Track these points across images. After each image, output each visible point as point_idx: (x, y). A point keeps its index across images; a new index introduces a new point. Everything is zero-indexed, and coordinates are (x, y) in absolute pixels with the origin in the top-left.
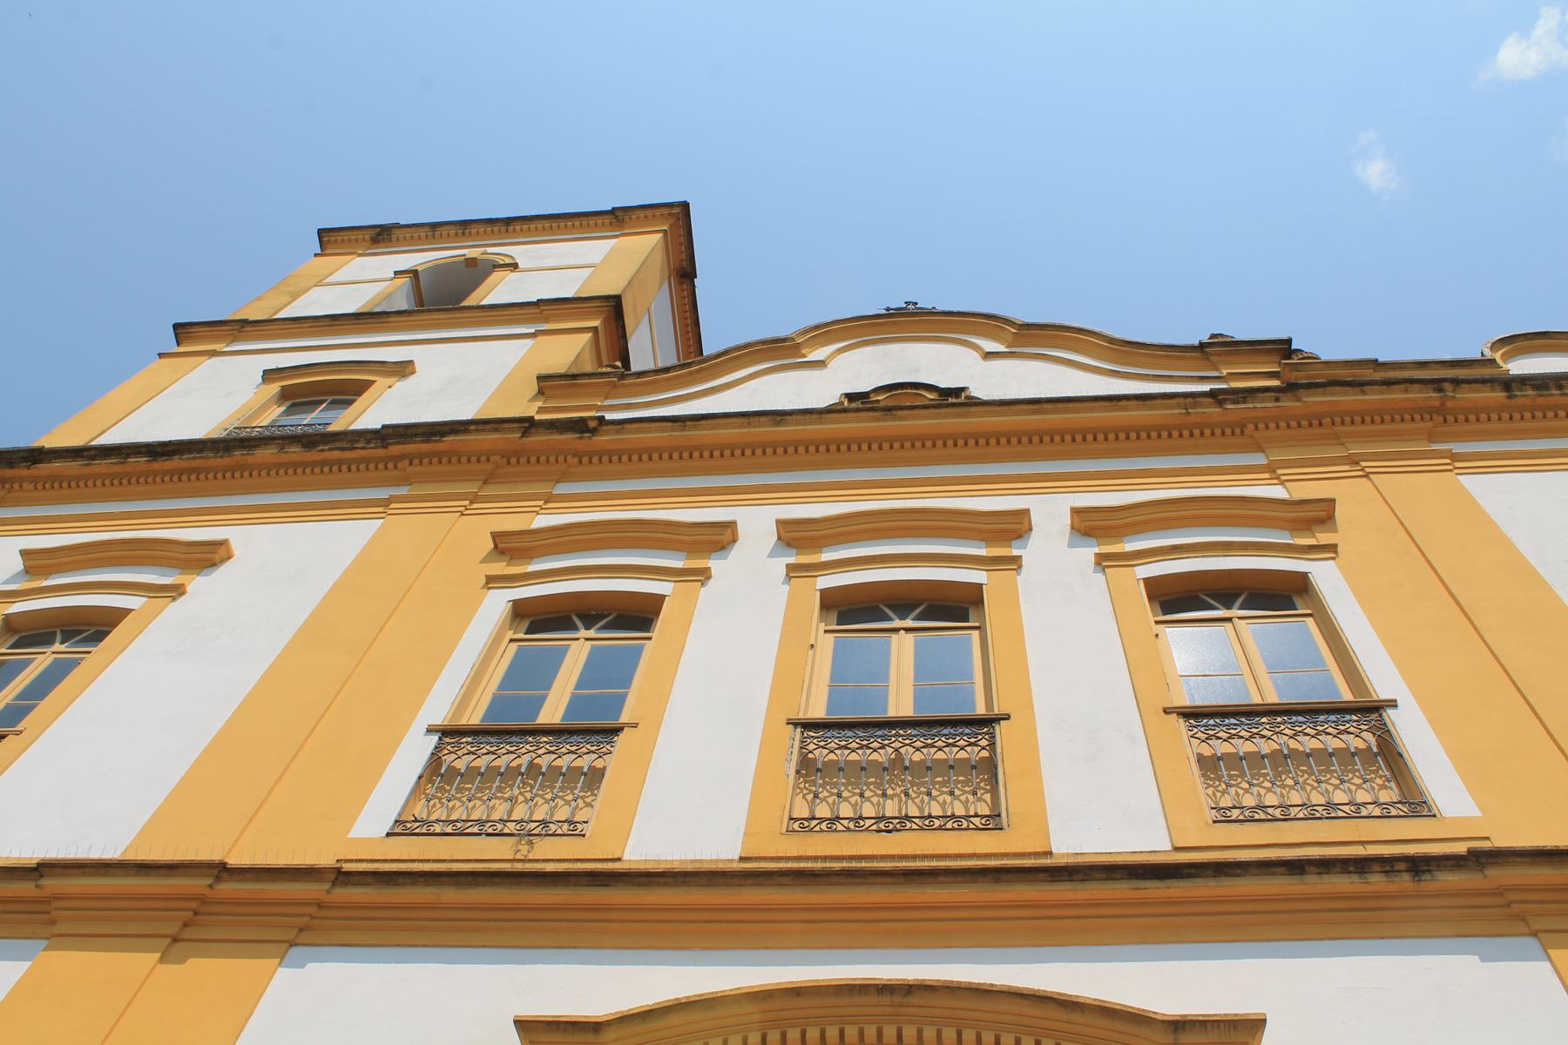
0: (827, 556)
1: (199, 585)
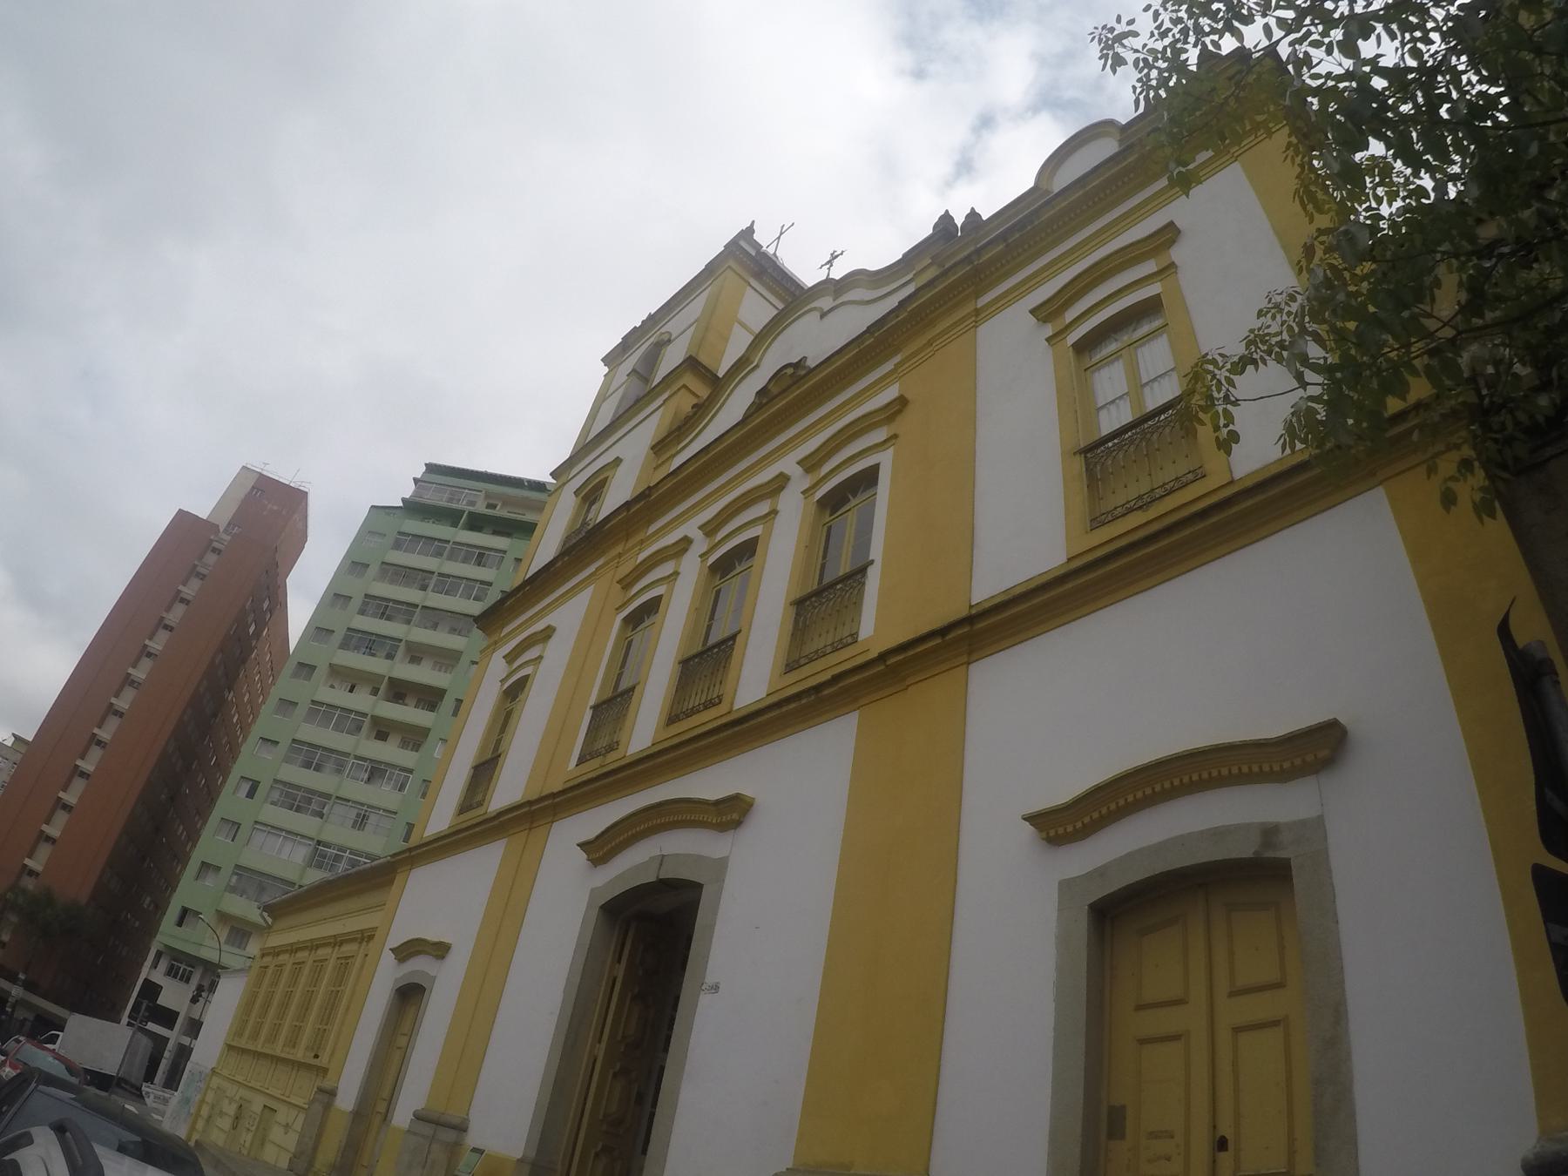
0: (1071, 315)
1: (1177, 254)
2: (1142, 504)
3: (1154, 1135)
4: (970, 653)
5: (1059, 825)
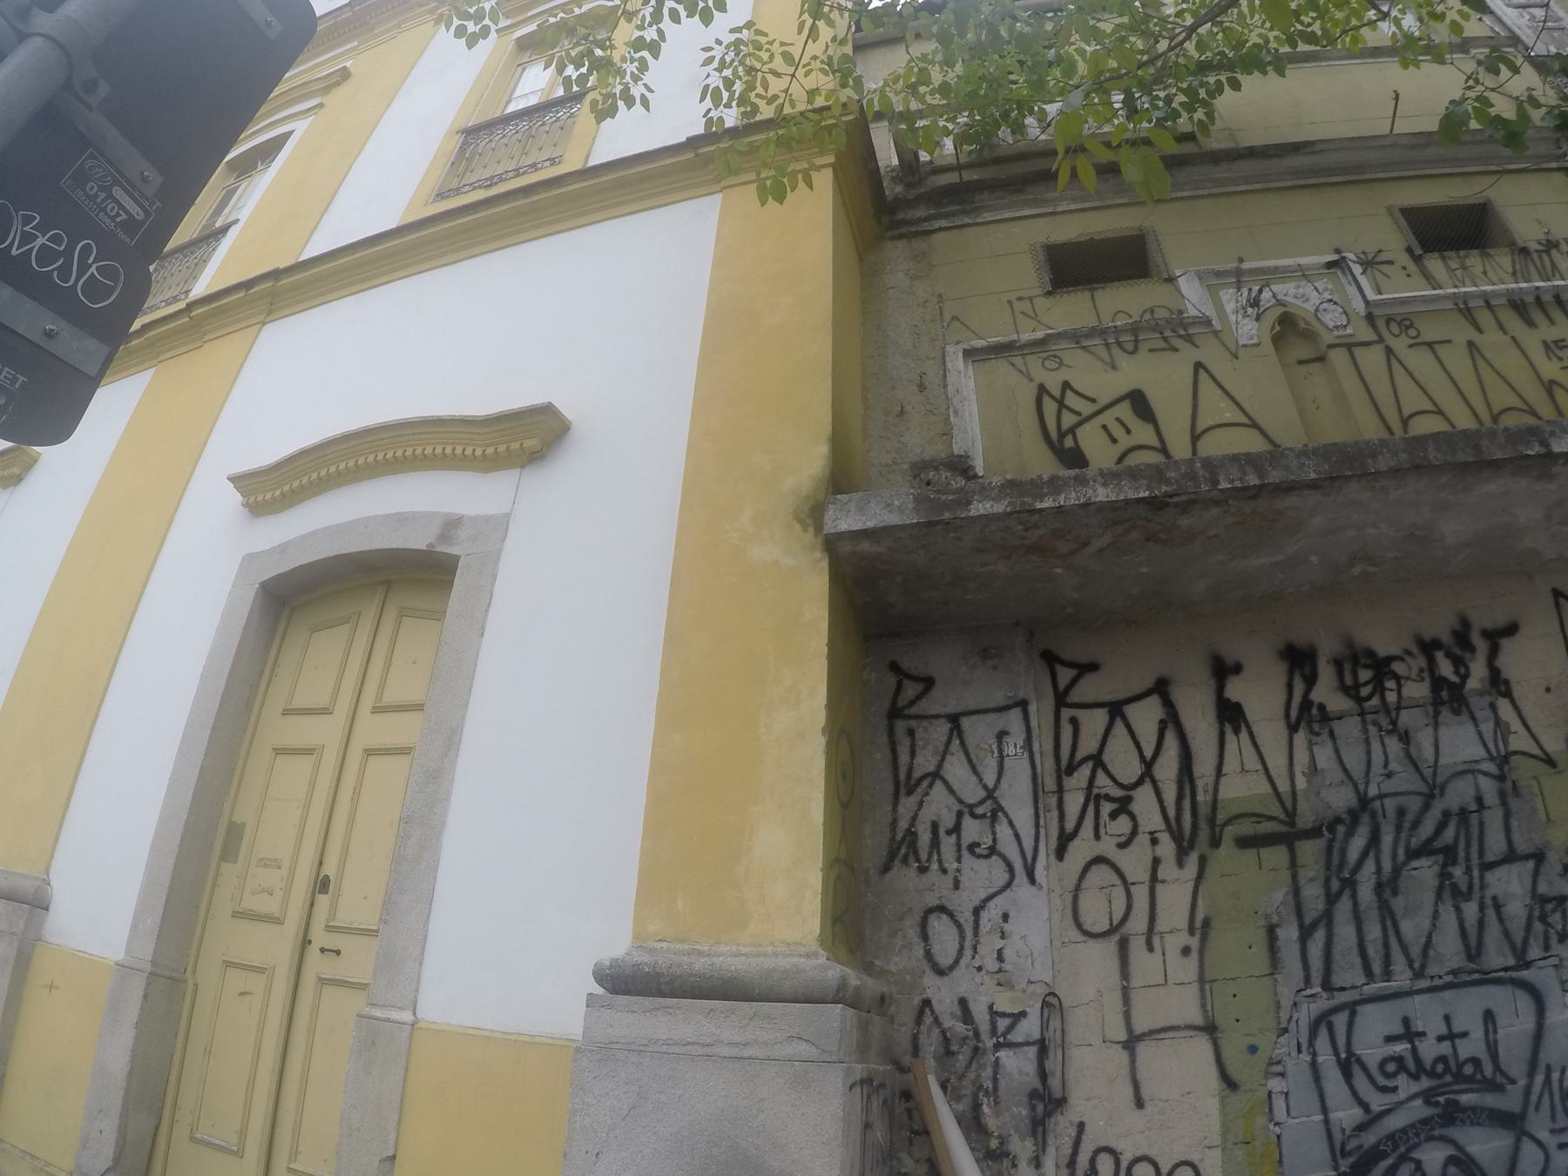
2: (490, 182)
3: (265, 863)
4: (269, 313)
5: (269, 489)
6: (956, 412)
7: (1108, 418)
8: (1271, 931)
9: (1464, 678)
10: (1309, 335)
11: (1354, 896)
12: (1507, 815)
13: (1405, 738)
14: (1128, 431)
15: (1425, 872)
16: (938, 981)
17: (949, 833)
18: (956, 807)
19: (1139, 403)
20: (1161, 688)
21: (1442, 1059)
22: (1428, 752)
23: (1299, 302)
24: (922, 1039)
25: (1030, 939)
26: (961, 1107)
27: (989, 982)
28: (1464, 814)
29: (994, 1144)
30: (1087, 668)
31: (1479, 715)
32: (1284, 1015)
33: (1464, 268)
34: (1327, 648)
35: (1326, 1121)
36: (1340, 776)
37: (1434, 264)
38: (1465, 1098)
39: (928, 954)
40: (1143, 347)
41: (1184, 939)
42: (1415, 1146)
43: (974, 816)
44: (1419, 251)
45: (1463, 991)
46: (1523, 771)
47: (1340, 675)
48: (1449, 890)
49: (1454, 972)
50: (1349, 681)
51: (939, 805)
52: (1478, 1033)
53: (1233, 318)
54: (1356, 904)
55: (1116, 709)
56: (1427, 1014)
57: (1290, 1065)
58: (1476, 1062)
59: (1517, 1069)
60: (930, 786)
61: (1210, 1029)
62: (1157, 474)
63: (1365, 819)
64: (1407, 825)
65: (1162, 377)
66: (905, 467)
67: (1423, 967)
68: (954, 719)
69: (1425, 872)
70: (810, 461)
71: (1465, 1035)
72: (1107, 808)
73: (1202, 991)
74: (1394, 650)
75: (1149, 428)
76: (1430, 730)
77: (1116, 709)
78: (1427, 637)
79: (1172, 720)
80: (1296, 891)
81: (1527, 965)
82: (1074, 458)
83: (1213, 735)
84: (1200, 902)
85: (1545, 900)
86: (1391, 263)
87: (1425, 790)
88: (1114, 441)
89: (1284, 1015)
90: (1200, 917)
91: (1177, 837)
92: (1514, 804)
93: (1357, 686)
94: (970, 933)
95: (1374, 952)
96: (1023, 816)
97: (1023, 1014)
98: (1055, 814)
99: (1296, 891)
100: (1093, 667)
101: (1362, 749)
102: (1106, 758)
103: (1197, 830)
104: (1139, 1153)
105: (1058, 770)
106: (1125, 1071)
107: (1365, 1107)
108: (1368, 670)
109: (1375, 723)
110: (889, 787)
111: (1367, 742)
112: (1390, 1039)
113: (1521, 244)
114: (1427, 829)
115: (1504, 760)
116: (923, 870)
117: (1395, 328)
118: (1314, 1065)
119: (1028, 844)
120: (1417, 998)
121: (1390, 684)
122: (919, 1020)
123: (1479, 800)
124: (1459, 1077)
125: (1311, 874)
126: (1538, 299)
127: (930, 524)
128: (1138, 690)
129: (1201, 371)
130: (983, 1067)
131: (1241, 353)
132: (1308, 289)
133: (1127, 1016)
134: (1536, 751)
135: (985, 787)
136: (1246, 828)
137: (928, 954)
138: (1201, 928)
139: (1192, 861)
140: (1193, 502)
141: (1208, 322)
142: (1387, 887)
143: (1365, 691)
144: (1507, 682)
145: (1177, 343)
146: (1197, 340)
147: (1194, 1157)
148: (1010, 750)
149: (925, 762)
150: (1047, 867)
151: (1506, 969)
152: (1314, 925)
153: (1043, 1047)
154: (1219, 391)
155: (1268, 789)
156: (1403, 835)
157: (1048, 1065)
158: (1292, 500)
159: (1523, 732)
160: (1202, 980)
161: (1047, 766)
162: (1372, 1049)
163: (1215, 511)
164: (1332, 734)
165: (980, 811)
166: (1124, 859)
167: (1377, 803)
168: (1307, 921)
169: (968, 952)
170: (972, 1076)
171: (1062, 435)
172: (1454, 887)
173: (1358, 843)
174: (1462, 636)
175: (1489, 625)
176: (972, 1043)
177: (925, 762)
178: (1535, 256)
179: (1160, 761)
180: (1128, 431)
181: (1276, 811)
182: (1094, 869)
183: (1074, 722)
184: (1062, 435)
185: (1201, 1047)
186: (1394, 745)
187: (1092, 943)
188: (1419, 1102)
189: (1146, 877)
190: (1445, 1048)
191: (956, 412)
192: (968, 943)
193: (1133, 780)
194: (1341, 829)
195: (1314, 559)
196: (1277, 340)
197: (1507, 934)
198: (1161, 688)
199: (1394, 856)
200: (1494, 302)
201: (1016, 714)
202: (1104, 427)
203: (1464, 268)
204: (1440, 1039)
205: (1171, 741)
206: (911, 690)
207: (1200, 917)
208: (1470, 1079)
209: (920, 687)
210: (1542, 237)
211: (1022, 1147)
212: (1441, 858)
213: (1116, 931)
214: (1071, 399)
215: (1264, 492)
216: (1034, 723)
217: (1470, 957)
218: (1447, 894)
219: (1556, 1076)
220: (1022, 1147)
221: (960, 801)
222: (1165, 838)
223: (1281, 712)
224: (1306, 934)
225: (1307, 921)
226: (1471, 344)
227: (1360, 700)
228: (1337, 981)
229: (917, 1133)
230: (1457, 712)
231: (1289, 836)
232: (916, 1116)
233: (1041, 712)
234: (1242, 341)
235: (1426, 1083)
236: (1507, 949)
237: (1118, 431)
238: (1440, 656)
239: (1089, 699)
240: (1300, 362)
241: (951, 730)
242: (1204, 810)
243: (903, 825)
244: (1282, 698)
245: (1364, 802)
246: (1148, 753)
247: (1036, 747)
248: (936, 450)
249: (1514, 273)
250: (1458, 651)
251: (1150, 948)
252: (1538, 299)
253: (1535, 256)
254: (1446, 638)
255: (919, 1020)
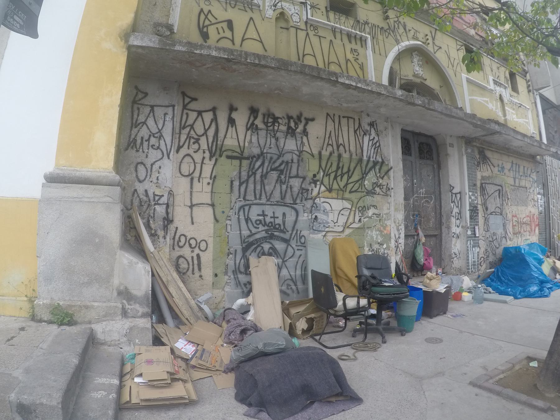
6: (173, 9)
7: (219, 26)
8: (232, 182)
9: (297, 128)
10: (287, 21)
11: (255, 177)
12: (298, 166)
13: (277, 139)
14: (224, 32)
15: (274, 175)
16: (139, 184)
17: (146, 141)
18: (149, 133)
19: (230, 24)
20: (214, 110)
21: (271, 222)
22: (282, 145)
23: (288, 10)
24: (134, 200)
25: (167, 175)
26: (144, 221)
27: (154, 186)
28: (287, 163)
29: (153, 232)
30: (194, 99)
31: (298, 139)
32: (232, 205)
33: (339, 19)
34: (262, 110)
35: (240, 233)
36: (258, 145)
37: (331, 15)
38: (275, 233)
39: (137, 176)
40: (237, 7)
41: (208, 180)
42: (262, 243)
43: (154, 137)
44: (329, 9)
45: (279, 207)
46: (305, 156)
47: (264, 118)
48: (279, 181)
49: (277, 202)
50: (266, 121)
51: (144, 132)
52: (281, 218)
53: (267, 8)
54: (255, 179)
55: (200, 113)
56: (269, 211)
57: (232, 217)
58: (279, 225)
59: (289, 229)
60: (142, 126)
61: (213, 205)
62: (231, 52)
63: (262, 158)
64: (272, 162)
65: (240, 18)
66: (152, 23)
67: (269, 199)
68: (152, 107)
69: (274, 175)
70: (128, 19)
71: (278, 218)
72: (192, 141)
73: (212, 195)
74: (280, 116)
75: (231, 33)
76: (284, 139)
77: (200, 113)
78: (290, 115)
79: (215, 119)
80: (240, 173)
81: (296, 204)
82: (205, 36)
83: (226, 126)
84: (214, 171)
85: (303, 189)
86: (319, 9)
87: (278, 153)
88: (219, 33)
89: (232, 205)
90: (213, 175)
91: (210, 152)
92: (301, 164)
93: (268, 122)
94: (149, 171)
95: (258, 192)
96: (168, 139)
97: (163, 196)
98: (178, 140)
99: (240, 173)
100: (196, 99)
101: (265, 139)
102: (194, 126)
103: (216, 151)
104: (192, 237)
105: (180, 128)
106: (189, 214)
107: (251, 231)
108: (272, 119)
109: (270, 133)
110: (130, 124)
111: (267, 138)
112: (258, 215)
113: (358, 19)
114: (277, 164)
115: (301, 152)
116: (137, 151)
117: (312, 28)
118: (239, 218)
119: (169, 147)
120: (267, 206)
121: (277, 124)
122: (133, 195)
123: (292, 160)
124: (275, 228)
125: (245, 169)
126: (355, 36)
127: (162, 49)
128: (207, 109)
129: (252, 22)
130: (151, 210)
131: (265, 19)
132: (292, 7)
133: (191, 199)
134: (310, 152)
135: (158, 129)
136: (230, 153)
137: (137, 176)
138: (214, 178)
139: (214, 160)
140: (238, 62)
141: (259, 7)
142: (264, 176)
143: (269, 125)
144: (307, 133)
145: (247, 9)
146: (254, 10)
147: (206, 239)
148: (167, 119)
149: (142, 119)
150: (173, 155)
151: (290, 204)
152: (243, 182)
153: (168, 205)
154: (254, 28)
155: (238, 144)
156: (271, 164)
157: (169, 211)
158: (266, 70)
159: (308, 146)
160: (212, 192)
161: (177, 125)
162: (254, 218)
163: (244, 66)
164: (258, 134)
165: (156, 135)
166: (195, 156)
167: (266, 155)
168: (242, 181)
169: (148, 177)
170: (147, 212)
171: (204, 27)
172: (281, 180)
173: (258, 164)
174: (299, 118)
175: (307, 117)
176: (148, 203)
177: (142, 119)
178: (361, 24)
179: (210, 130)
180: (224, 32)
181: (238, 150)
182: (186, 157)
183: (187, 114)
184: (204, 27)
185: (210, 210)
186: (273, 140)
187: (183, 178)
188: (264, 232)
189: (200, 162)
190: (272, 220)
191: (173, 9)
192: (149, 174)
193: (201, 134)
194: (255, 159)
195: (266, 86)
196: (277, 19)
197: (292, 195)
198: (214, 110)
199: (267, 169)
200: (357, 37)
201: (171, 108)
202: (217, 28)
203: (339, 19)
204: (271, 217)
205: (213, 125)
206: (140, 96)
207: (213, 175)
208: (277, 229)
209: (143, 95)
210: (365, 20)
211: (161, 233)
212: (279, 172)
213: (190, 175)
214: (210, 17)
215: (258, 65)
216: (176, 112)
217: (282, 199)
218: (279, 182)
219: (299, 232)
220: (161, 233)
221: (150, 132)
222: (207, 152)
223: (245, 124)
224: (241, 184)
225: (242, 181)
226: (331, 40)
227: (267, 126)
228: (247, 198)
229: (132, 228)
230: (292, 137)
231: (241, 158)
232: (132, 223)
233: (178, 109)
234: (267, 16)
235: (266, 228)
236: (291, 199)
237: (221, 31)
238: (292, 121)
239: (192, 108)
240: (281, 28)
241: (151, 111)
242: (219, 146)
243: (133, 137)
244: (246, 121)
245: (262, 153)
246: (207, 128)
247: (175, 119)
248: (163, 20)
249: (352, 26)
250: (297, 121)
251: (199, 182)
252: (355, 36)
253: (361, 24)
254: (295, 117)
255: (133, 195)
